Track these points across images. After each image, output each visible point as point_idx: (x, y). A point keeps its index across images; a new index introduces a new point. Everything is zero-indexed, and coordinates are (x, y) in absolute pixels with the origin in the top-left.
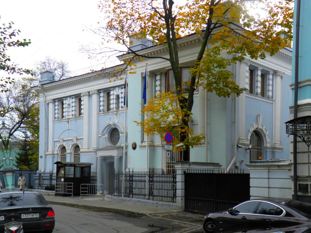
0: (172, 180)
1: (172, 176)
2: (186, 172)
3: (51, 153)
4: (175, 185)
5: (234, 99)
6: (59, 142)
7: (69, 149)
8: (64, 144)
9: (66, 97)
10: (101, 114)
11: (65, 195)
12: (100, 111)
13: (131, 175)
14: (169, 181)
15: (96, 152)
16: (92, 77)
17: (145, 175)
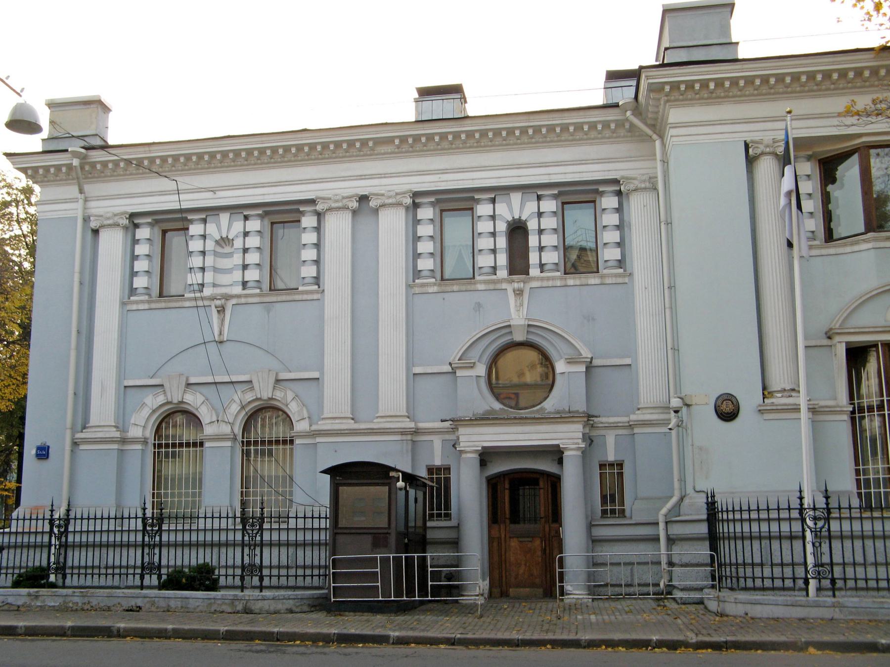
12: (417, 274)
14: (732, 535)
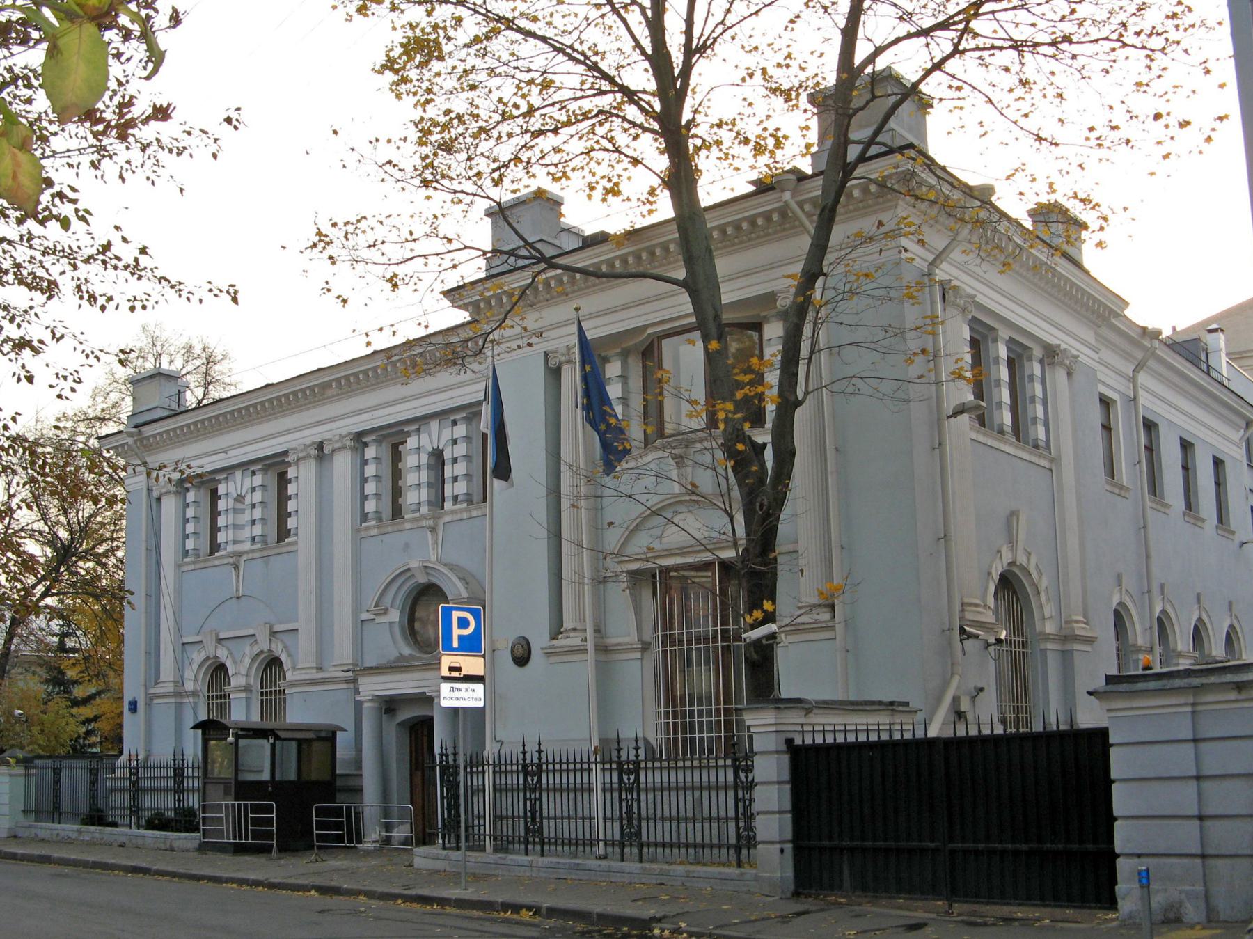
0: (615, 779)
1: (520, 768)
2: (798, 741)
3: (170, 688)
4: (747, 797)
5: (940, 444)
6: (199, 646)
7: (242, 674)
8: (222, 654)
9: (230, 469)
10: (366, 529)
11: (240, 849)
12: (364, 517)
13: (532, 764)
15: (355, 681)
16: (334, 384)
17: (585, 766)
